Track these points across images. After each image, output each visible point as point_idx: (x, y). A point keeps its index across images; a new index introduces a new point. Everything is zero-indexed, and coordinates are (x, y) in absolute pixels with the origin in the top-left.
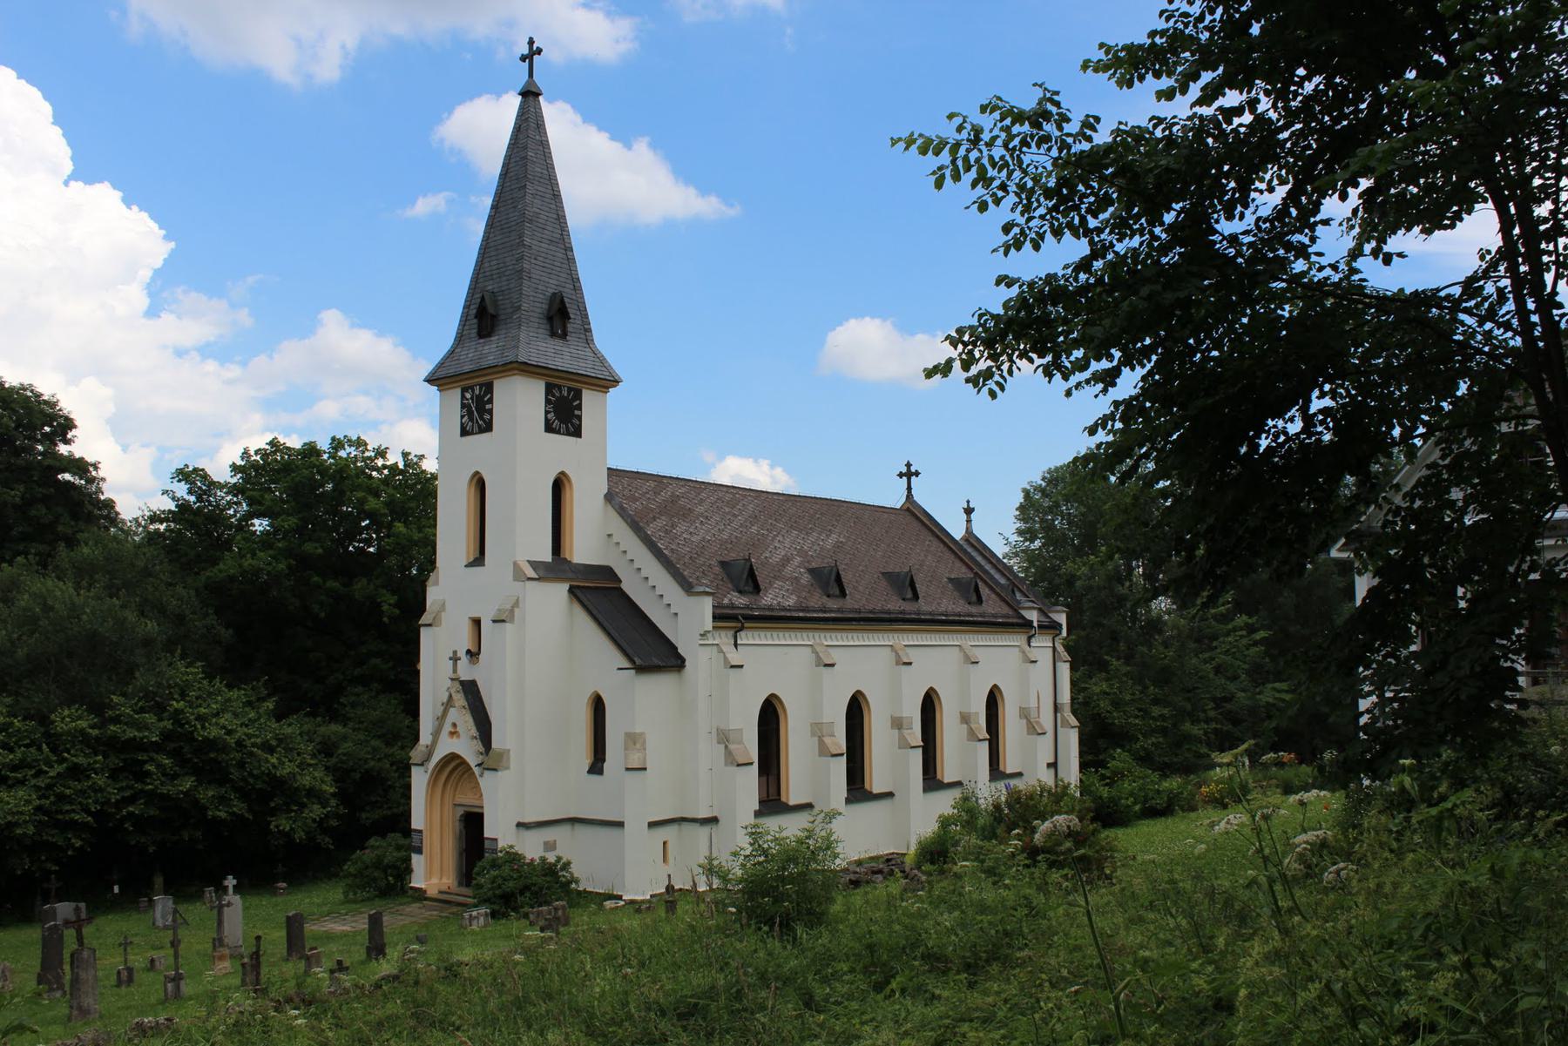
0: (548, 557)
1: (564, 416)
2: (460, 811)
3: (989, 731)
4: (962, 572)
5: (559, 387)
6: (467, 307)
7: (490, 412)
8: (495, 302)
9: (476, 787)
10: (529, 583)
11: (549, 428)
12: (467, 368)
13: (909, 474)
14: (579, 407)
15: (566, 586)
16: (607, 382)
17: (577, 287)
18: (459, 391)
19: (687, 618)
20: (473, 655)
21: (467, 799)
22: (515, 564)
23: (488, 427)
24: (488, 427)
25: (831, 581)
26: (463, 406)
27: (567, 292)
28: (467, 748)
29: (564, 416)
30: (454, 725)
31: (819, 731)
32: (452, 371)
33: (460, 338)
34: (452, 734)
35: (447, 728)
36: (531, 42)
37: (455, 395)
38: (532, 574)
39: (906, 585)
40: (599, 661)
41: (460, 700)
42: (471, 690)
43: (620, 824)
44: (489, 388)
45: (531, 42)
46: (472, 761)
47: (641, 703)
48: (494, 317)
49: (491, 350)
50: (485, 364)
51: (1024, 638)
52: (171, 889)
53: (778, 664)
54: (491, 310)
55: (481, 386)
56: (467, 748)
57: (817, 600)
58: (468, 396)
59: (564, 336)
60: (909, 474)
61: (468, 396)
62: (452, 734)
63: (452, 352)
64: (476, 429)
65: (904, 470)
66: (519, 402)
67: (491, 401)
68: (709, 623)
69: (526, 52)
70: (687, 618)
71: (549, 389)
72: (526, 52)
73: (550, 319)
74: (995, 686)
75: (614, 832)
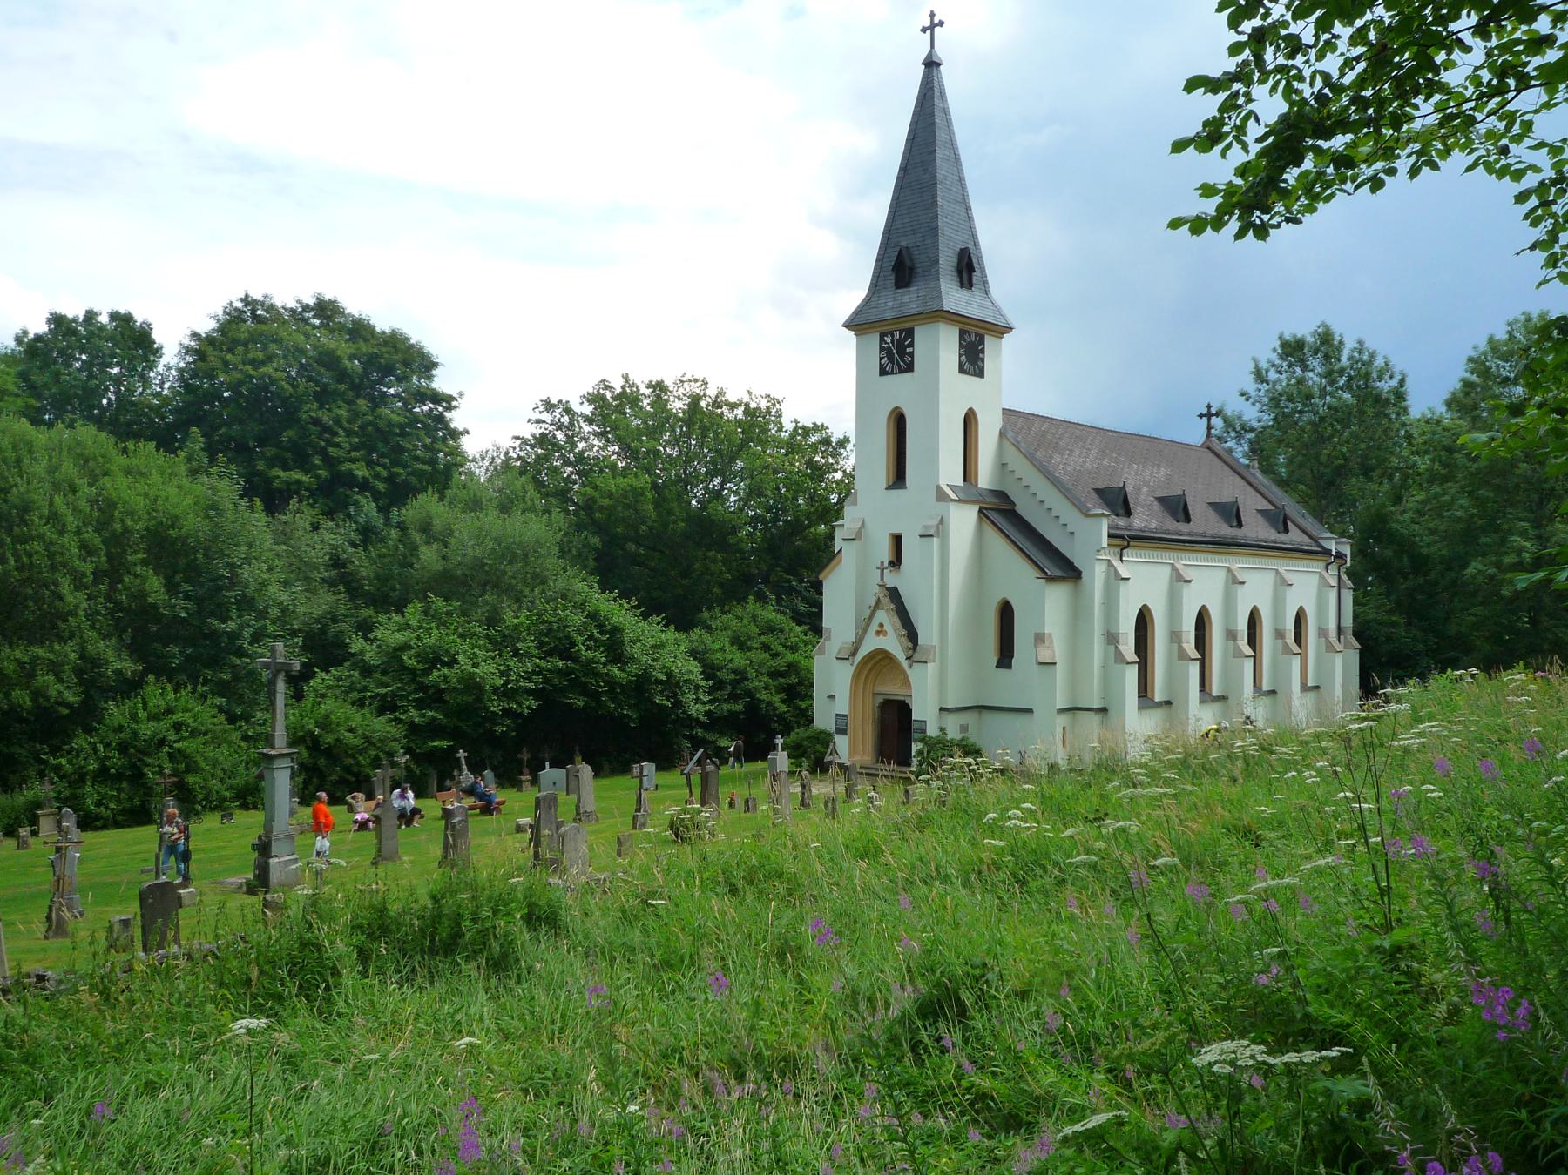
0: (961, 483)
1: (972, 360)
2: (880, 699)
3: (1137, 651)
4: (1266, 506)
5: (969, 333)
6: (880, 260)
7: (911, 355)
8: (910, 254)
9: (907, 682)
10: (952, 505)
11: (962, 370)
12: (889, 315)
13: (932, 27)
14: (982, 351)
15: (977, 508)
16: (1001, 330)
17: (976, 244)
18: (877, 337)
19: (1088, 537)
20: (896, 562)
21: (893, 690)
22: (939, 488)
23: (910, 368)
24: (910, 368)
25: (1178, 508)
26: (882, 349)
27: (971, 247)
28: (893, 644)
29: (972, 360)
30: (881, 625)
31: (1175, 636)
32: (873, 318)
33: (875, 287)
34: (878, 633)
35: (874, 627)
36: (932, 15)
37: (875, 339)
38: (953, 496)
39: (1232, 513)
40: (1015, 575)
41: (886, 601)
42: (894, 594)
43: (1030, 711)
44: (910, 333)
45: (932, 15)
46: (901, 656)
47: (1047, 610)
48: (912, 269)
49: (911, 299)
50: (907, 312)
51: (1323, 564)
52: (558, 763)
53: (1144, 580)
54: (908, 263)
55: (901, 332)
56: (893, 644)
57: (1171, 525)
58: (888, 340)
59: (971, 286)
60: (932, 27)
61: (888, 340)
62: (878, 633)
63: (867, 302)
64: (896, 369)
65: (1205, 411)
66: (940, 349)
67: (912, 345)
68: (1105, 541)
69: (937, 29)
70: (1088, 537)
71: (962, 333)
72: (928, 24)
73: (960, 272)
74: (1145, 606)
75: (1019, 720)
